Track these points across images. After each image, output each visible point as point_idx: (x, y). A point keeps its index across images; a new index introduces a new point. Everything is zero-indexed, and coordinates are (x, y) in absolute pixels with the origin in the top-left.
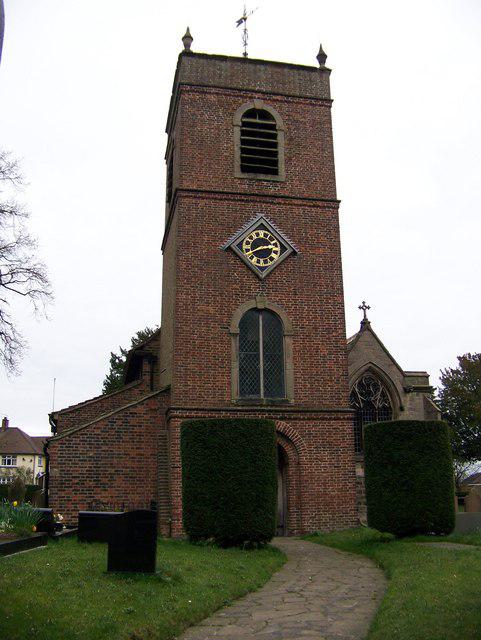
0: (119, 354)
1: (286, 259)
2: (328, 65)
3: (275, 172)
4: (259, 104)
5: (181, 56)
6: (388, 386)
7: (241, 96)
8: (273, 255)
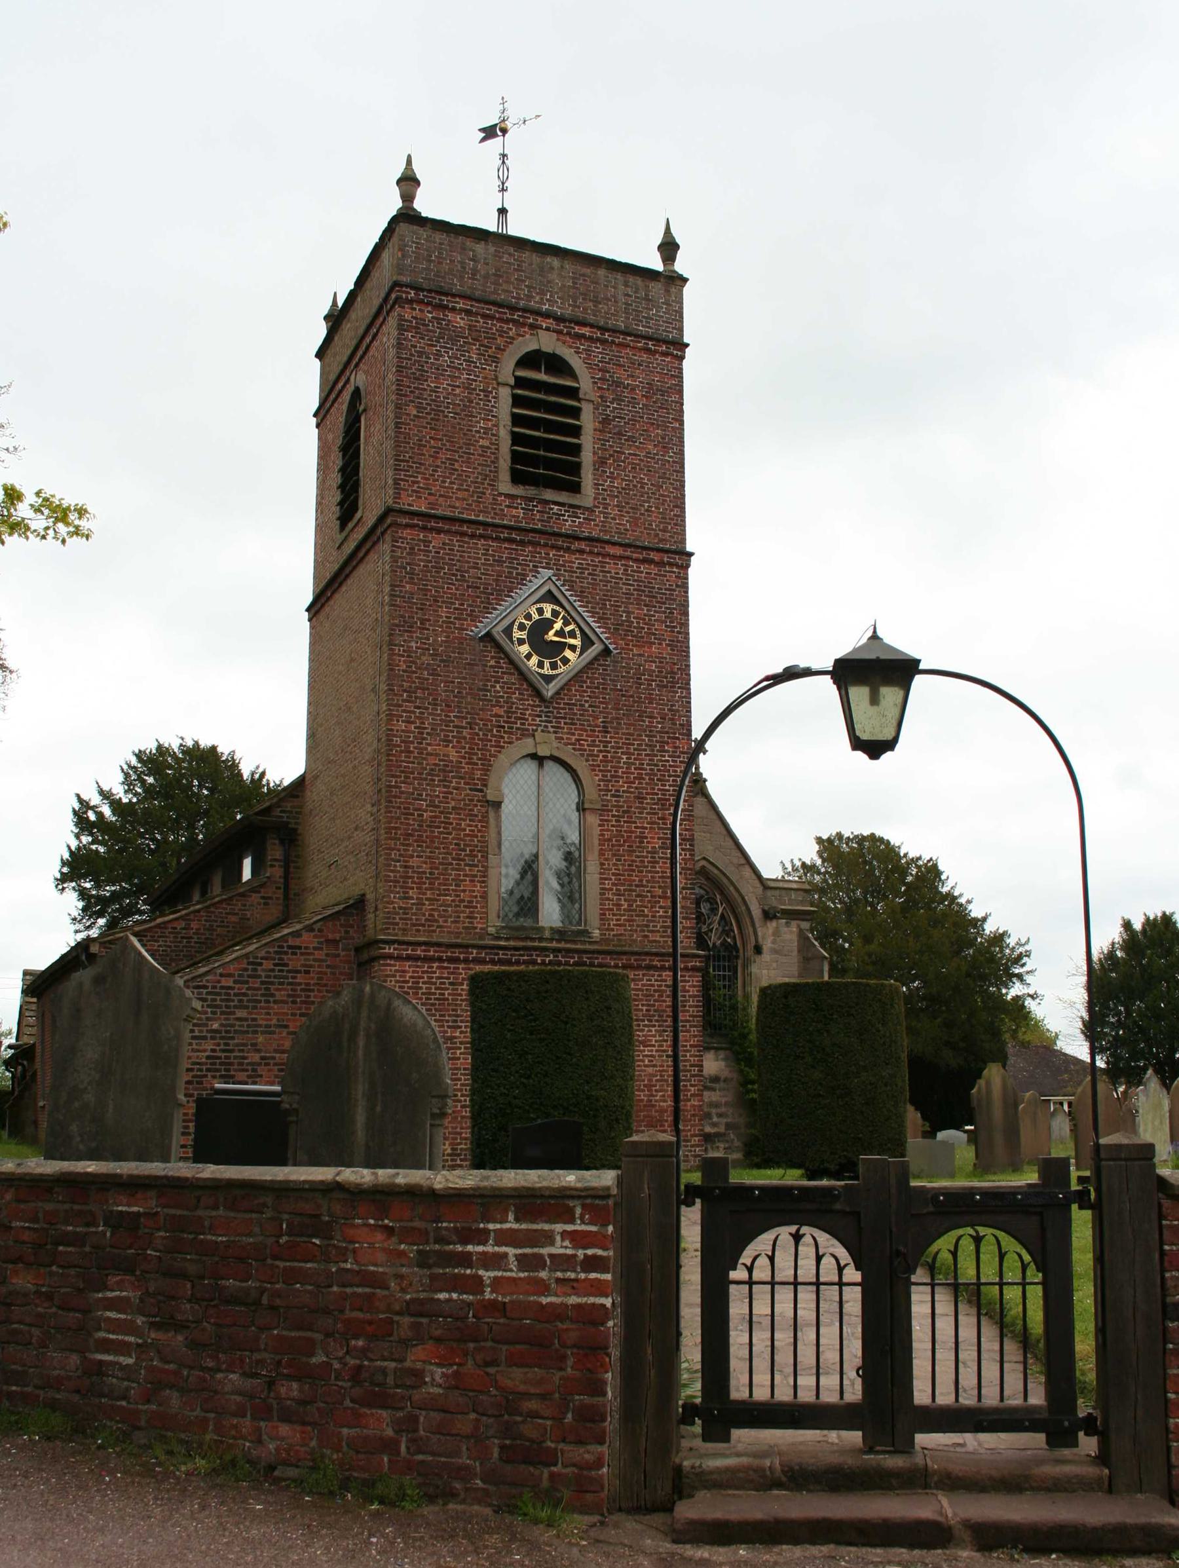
0: (95, 800)
1: (591, 663)
2: (680, 266)
3: (575, 488)
4: (547, 342)
5: (394, 221)
6: (735, 908)
7: (514, 321)
8: (568, 653)
